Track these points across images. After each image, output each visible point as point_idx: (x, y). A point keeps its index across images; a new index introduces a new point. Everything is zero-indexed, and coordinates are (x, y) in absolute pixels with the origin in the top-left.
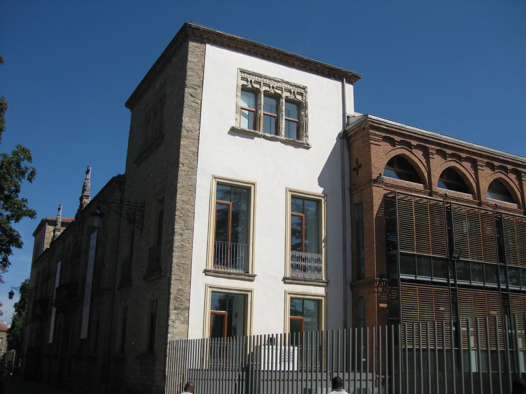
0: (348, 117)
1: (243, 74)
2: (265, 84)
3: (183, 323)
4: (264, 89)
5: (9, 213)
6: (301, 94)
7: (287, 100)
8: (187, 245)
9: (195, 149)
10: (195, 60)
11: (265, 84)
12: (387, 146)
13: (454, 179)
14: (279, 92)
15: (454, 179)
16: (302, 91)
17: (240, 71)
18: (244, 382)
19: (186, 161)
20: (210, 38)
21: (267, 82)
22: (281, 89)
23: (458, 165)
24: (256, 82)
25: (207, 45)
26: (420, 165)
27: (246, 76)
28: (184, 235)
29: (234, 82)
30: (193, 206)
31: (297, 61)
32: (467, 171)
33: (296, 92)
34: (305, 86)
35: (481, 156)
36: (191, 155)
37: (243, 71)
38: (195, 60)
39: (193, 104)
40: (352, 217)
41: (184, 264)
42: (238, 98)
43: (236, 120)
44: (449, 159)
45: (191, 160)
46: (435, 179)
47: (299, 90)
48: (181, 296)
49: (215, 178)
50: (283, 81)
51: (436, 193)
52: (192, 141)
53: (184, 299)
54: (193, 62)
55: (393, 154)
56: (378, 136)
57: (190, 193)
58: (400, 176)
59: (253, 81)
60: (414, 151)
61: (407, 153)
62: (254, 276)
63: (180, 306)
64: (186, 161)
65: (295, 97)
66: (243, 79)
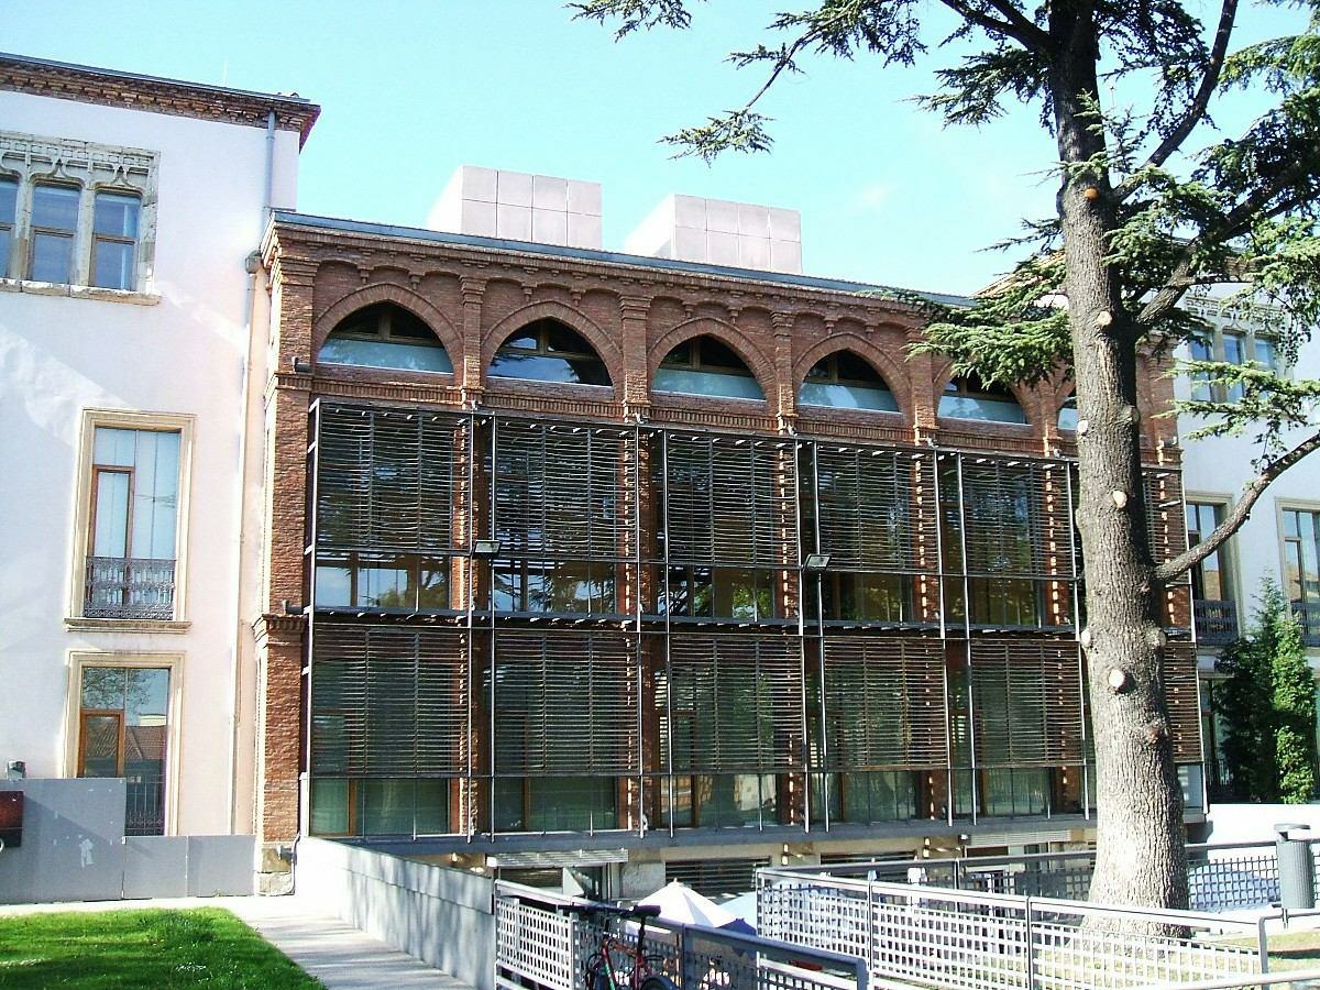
6: (144, 173)
7: (39, 182)
14: (74, 173)
33: (126, 170)
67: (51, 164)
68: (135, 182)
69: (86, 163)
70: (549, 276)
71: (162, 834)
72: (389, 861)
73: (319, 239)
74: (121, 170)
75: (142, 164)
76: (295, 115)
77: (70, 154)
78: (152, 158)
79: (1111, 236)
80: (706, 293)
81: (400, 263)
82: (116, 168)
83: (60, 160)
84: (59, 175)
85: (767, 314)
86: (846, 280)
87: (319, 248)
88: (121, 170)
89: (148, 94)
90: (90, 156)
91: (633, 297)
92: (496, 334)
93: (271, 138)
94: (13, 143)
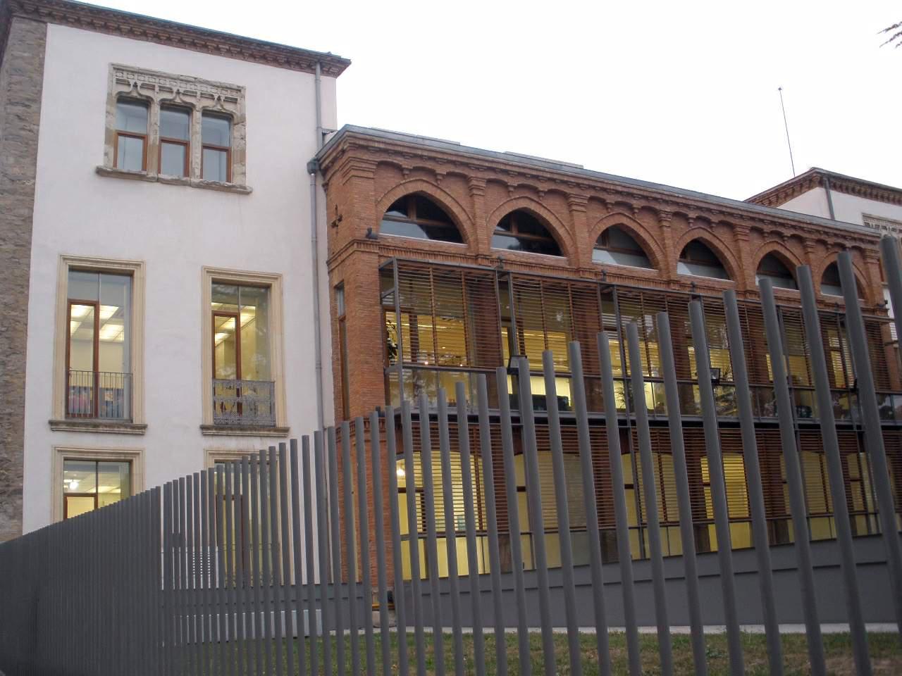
1: (119, 74)
2: (162, 89)
3: (12, 518)
4: (158, 97)
6: (234, 101)
7: (206, 113)
8: (15, 381)
9: (25, 212)
10: (26, 55)
11: (162, 89)
12: (757, 241)
14: (188, 99)
15: (832, 276)
17: (114, 68)
19: (11, 235)
20: (54, 13)
21: (168, 84)
22: (193, 94)
25: (49, 24)
27: (125, 76)
28: (10, 364)
29: (100, 88)
30: (25, 311)
31: (224, 44)
32: (795, 256)
33: (222, 98)
34: (241, 85)
36: (20, 223)
37: (118, 69)
38: (26, 55)
39: (23, 133)
40: (333, 311)
41: (10, 414)
43: (106, 154)
45: (19, 231)
47: (229, 94)
48: (7, 470)
49: (65, 259)
50: (196, 81)
52: (21, 198)
53: (11, 475)
54: (22, 58)
55: (688, 239)
56: (366, 161)
57: (19, 289)
58: (526, 245)
59: (139, 84)
60: (788, 245)
61: (707, 236)
62: (145, 427)
63: (6, 489)
64: (11, 235)
65: (222, 106)
66: (119, 82)
68: (229, 107)
70: (386, 156)
71: (418, 414)
74: (219, 99)
75: (235, 93)
76: (332, 65)
77: (185, 86)
79: (689, 643)
80: (618, 195)
81: (429, 165)
82: (216, 97)
83: (178, 90)
84: (178, 100)
85: (565, 196)
88: (219, 99)
89: (236, 46)
90: (199, 88)
91: (578, 196)
92: (493, 218)
93: (317, 81)
94: (147, 77)
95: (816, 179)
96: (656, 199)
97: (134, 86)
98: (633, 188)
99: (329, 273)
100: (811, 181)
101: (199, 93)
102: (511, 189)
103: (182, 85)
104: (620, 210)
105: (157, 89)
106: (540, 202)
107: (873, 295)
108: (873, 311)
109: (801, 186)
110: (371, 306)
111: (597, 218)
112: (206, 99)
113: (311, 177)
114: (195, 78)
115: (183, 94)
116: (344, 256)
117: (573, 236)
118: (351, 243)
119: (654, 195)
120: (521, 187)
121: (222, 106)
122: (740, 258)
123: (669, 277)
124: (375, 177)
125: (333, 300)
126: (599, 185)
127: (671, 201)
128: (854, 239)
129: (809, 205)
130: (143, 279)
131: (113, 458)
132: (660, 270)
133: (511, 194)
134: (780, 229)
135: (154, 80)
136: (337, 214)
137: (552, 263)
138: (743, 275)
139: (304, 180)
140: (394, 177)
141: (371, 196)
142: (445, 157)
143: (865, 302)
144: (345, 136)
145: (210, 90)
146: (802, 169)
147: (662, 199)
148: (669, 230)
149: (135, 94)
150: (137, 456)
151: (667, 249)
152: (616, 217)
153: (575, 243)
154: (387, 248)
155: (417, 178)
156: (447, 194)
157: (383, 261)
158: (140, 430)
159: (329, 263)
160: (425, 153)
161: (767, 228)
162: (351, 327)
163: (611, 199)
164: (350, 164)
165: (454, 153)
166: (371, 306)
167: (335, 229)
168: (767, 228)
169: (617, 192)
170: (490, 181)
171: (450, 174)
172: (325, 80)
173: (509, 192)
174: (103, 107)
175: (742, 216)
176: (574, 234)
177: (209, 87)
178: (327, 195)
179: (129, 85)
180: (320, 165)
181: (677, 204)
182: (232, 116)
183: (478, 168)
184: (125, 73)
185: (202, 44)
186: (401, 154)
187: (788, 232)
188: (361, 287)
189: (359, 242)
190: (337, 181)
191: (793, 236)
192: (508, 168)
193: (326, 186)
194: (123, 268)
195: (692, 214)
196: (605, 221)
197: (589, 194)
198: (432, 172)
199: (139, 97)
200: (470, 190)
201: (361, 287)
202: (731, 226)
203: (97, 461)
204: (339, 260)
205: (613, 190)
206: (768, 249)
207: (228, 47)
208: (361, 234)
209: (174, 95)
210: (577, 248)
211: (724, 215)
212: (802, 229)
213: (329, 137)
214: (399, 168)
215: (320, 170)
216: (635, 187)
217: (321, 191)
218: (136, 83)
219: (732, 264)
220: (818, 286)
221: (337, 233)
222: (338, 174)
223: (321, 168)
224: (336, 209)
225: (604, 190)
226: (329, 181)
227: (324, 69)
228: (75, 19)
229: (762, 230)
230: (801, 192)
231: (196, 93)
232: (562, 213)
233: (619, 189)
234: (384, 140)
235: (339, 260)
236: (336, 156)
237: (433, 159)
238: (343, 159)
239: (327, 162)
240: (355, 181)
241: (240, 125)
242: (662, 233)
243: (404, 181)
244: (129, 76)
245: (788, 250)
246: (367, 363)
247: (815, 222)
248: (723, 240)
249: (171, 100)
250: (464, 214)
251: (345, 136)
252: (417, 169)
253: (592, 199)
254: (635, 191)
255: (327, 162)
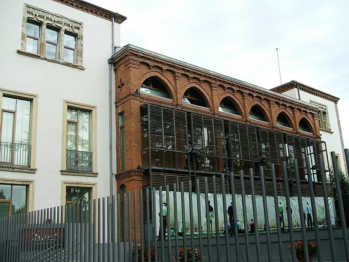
0: (115, 48)
4: (46, 22)
5: (193, 152)
6: (78, 29)
13: (257, 111)
14: (42, 20)
15: (283, 118)
16: (79, 26)
18: (211, 230)
21: (50, 16)
22: (61, 23)
23: (198, 86)
24: (75, 27)
26: (169, 85)
27: (31, 10)
33: (73, 27)
35: (178, 68)
37: (28, 7)
42: (24, 28)
44: (281, 107)
46: (275, 119)
47: (76, 25)
50: (62, 17)
51: (299, 133)
55: (148, 76)
59: (37, 15)
65: (73, 30)
66: (28, 12)
67: (52, 21)
68: (76, 31)
69: (62, 22)
72: (325, 218)
73: (140, 54)
74: (72, 27)
75: (79, 25)
76: (120, 19)
78: (81, 24)
80: (229, 85)
81: (160, 65)
82: (71, 26)
83: (54, 20)
86: (335, 97)
87: (140, 57)
89: (80, 5)
95: (292, 85)
96: (242, 88)
97: (35, 15)
98: (186, 67)
99: (116, 107)
100: (292, 86)
101: (63, 23)
102: (190, 79)
103: (56, 18)
104: (304, 113)
105: (45, 18)
106: (201, 85)
107: (316, 132)
108: (316, 138)
109: (288, 87)
110: (137, 122)
111: (220, 93)
112: (66, 26)
113: (110, 65)
114: (62, 16)
115: (57, 22)
116: (125, 100)
117: (212, 99)
118: (129, 95)
119: (242, 86)
120: (194, 78)
121: (73, 30)
122: (271, 113)
123: (246, 119)
124: (139, 68)
125: (117, 119)
126: (223, 80)
127: (248, 89)
128: (310, 109)
129: (292, 94)
130: (37, 102)
131: (20, 183)
132: (243, 116)
133: (190, 81)
134: (285, 103)
135: (44, 14)
136: (121, 82)
137: (204, 110)
138: (272, 121)
139: (107, 66)
140: (146, 69)
141: (137, 75)
142: (167, 62)
143: (313, 134)
144: (128, 49)
145: (68, 22)
146: (286, 81)
147: (244, 88)
148: (247, 100)
149: (35, 19)
150: (32, 183)
151: (246, 108)
152: (228, 93)
153: (213, 103)
154: (142, 98)
155: (155, 70)
156: (166, 78)
157: (141, 104)
158: (33, 171)
159: (116, 103)
160: (159, 60)
161: (281, 103)
162: (128, 131)
163: (226, 86)
164: (129, 62)
165: (170, 61)
166: (137, 122)
167: (120, 89)
168: (281, 103)
169: (229, 83)
170: (182, 74)
171: (168, 70)
172: (116, 24)
173: (189, 79)
174: (21, 23)
175: (272, 97)
176: (213, 99)
177: (68, 21)
178: (116, 74)
179: (33, 15)
180: (114, 61)
181: (250, 90)
182: (77, 35)
183: (178, 68)
184: (31, 9)
185: (81, 7)
186: (149, 59)
187: (288, 105)
188: (133, 114)
189: (133, 95)
190: (122, 68)
191: (290, 107)
192: (189, 69)
193: (115, 70)
194: (28, 97)
195: (255, 95)
196: (223, 95)
197: (219, 83)
198: (161, 68)
199: (37, 21)
200: (211, 87)
201: (133, 114)
202: (268, 101)
203: (12, 185)
204: (122, 102)
205: (146, 57)
206: (281, 111)
207: (76, 5)
208: (133, 91)
209: (53, 22)
210: (213, 105)
211: (230, 85)
212: (293, 104)
213: (118, 50)
214: (148, 65)
215: (113, 63)
216: (235, 82)
217: (113, 72)
218: (36, 14)
219: (268, 116)
220: (298, 127)
221: (121, 91)
222: (122, 65)
223: (114, 62)
224: (121, 80)
225: (224, 82)
226: (117, 68)
227: (116, 20)
228: (70, 3)
229: (307, 111)
230: (288, 90)
231: (62, 22)
232: (208, 90)
233: (230, 82)
234: (143, 53)
235: (122, 102)
236: (122, 57)
237: (162, 63)
238: (123, 60)
239: (117, 60)
240: (131, 68)
241: (81, 40)
242: (244, 101)
243: (150, 71)
244: (33, 10)
245: (288, 112)
246: (135, 146)
247: (297, 102)
248: (265, 106)
249: (51, 24)
250: (172, 87)
251: (128, 49)
252: (155, 66)
253: (219, 85)
254: (235, 84)
255: (117, 60)
